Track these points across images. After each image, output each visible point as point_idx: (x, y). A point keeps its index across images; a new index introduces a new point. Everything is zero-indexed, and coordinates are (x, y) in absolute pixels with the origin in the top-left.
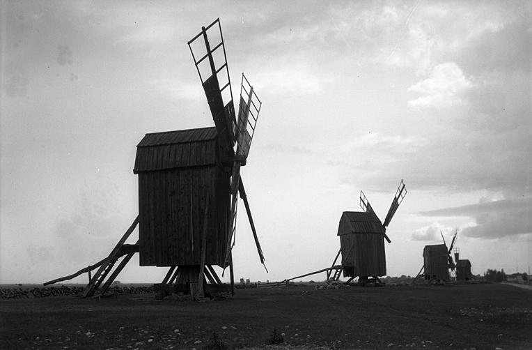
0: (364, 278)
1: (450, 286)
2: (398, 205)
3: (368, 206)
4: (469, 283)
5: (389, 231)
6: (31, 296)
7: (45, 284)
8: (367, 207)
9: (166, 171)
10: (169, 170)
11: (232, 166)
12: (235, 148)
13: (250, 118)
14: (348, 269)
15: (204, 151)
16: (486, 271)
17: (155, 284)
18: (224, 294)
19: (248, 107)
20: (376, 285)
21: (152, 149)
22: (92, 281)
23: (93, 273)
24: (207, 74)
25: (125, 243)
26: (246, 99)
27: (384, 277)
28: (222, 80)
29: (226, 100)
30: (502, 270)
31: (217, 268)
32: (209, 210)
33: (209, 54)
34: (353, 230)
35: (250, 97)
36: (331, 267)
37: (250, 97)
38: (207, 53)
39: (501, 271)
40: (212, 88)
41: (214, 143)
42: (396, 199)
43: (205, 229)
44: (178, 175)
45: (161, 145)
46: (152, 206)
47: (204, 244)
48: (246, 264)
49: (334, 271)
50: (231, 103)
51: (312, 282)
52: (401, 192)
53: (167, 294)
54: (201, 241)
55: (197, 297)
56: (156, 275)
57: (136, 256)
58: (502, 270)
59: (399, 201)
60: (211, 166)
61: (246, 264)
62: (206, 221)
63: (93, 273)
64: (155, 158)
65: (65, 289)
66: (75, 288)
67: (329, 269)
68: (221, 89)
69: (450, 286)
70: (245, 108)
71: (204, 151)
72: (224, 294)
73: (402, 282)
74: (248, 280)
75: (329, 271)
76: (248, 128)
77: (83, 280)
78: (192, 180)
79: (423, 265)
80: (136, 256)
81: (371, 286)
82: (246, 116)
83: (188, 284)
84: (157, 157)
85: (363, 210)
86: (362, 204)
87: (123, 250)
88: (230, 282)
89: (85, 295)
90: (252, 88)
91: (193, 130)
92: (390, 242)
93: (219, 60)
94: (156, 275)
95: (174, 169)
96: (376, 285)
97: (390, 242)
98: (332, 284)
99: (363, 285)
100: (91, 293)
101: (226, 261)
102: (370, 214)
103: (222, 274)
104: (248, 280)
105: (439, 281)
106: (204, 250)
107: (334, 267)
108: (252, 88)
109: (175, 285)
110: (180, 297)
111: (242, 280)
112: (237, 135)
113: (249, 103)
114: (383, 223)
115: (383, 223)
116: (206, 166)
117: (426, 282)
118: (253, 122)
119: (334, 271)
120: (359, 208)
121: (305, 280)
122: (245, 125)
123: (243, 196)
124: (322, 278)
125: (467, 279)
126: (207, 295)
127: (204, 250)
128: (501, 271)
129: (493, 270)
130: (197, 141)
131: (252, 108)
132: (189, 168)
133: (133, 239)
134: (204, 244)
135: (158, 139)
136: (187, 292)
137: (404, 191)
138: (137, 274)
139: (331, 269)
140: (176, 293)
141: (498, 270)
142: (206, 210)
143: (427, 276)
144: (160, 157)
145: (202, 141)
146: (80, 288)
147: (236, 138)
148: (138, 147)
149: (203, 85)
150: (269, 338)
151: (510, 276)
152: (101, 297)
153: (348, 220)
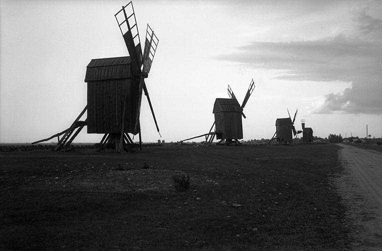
0: (229, 140)
1: (293, 146)
2: (250, 95)
3: (233, 95)
4: (311, 144)
5: (245, 111)
6: (20, 151)
7: (32, 144)
8: (232, 95)
9: (103, 81)
10: (104, 80)
11: (140, 78)
12: (142, 68)
13: (151, 49)
14: (219, 135)
15: (124, 70)
16: (329, 135)
17: (96, 144)
18: (135, 149)
19: (150, 43)
20: (237, 145)
21: (95, 68)
22: (60, 142)
23: (61, 137)
24: (125, 30)
25: (79, 120)
26: (149, 39)
27: (241, 140)
28: (134, 32)
29: (136, 43)
30: (340, 135)
31: (131, 135)
32: (126, 102)
33: (127, 20)
34: (222, 110)
35: (152, 37)
36: (208, 133)
37: (152, 37)
38: (125, 19)
39: (339, 135)
40: (128, 38)
41: (130, 66)
42: (249, 91)
43: (124, 113)
44: (110, 83)
45: (100, 66)
46: (95, 100)
47: (123, 122)
48: (149, 133)
49: (210, 136)
50: (140, 44)
51: (193, 143)
52: (252, 87)
53: (103, 149)
54: (122, 119)
55: (119, 151)
56: (96, 138)
57: (85, 127)
58: (340, 135)
59: (250, 92)
60: (127, 78)
61: (149, 133)
62: (124, 108)
63: (61, 137)
64: (97, 73)
65: (41, 147)
66: (46, 146)
67: (207, 134)
68: (133, 37)
69: (293, 146)
70: (148, 45)
71: (124, 70)
72: (135, 149)
73: (264, 143)
74: (163, 141)
75: (207, 136)
76: (150, 56)
77: (55, 140)
78: (117, 86)
79: (275, 131)
80: (85, 127)
81: (233, 145)
82: (149, 49)
83: (114, 143)
84: (98, 73)
85: (228, 97)
86: (229, 93)
87: (78, 124)
88: (139, 141)
89: (56, 150)
90: (153, 32)
91: (118, 58)
92: (245, 117)
93: (132, 22)
94: (96, 138)
95: (108, 80)
96: (237, 145)
97: (245, 117)
98: (206, 147)
99: (228, 145)
100: (59, 149)
101: (137, 130)
102: (234, 100)
103: (135, 139)
104: (163, 141)
105: (286, 142)
106: (123, 124)
107: (210, 133)
108: (153, 32)
109: (107, 144)
110: (110, 151)
111: (159, 141)
112: (143, 61)
113: (151, 41)
114: (241, 106)
115: (241, 106)
116: (125, 79)
117: (278, 143)
118: (156, 41)
119: (210, 136)
120: (227, 96)
121: (191, 141)
122: (148, 54)
123: (147, 94)
124: (203, 139)
125: (310, 141)
126: (125, 150)
127: (123, 124)
128: (339, 135)
129: (334, 134)
130: (120, 65)
131: (153, 44)
132: (116, 79)
133: (84, 118)
134: (123, 122)
135: (99, 62)
136: (114, 148)
137: (253, 86)
138: (85, 137)
139: (209, 134)
140: (108, 148)
141: (337, 135)
142: (125, 103)
143: (278, 139)
144: (100, 73)
145: (124, 65)
146: (22, 146)
147: (143, 62)
148: (88, 67)
149: (123, 36)
150: (143, 166)
151: (346, 139)
152: (65, 151)
153: (219, 104)
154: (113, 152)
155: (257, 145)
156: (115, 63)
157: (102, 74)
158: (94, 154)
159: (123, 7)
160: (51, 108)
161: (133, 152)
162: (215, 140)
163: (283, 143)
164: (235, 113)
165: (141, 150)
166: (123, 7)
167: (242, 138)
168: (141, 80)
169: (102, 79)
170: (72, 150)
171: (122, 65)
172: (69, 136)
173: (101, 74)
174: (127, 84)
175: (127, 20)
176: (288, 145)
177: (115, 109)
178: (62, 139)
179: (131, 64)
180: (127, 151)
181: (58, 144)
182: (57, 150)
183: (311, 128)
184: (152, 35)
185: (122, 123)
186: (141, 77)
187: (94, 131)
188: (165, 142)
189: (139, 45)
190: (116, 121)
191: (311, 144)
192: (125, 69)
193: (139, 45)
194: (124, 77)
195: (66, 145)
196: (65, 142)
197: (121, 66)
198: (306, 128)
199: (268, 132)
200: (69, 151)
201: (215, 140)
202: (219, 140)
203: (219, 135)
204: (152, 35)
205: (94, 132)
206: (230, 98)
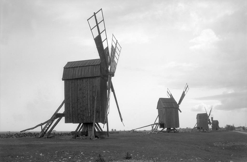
0: (169, 129)
2: (185, 95)
3: (171, 95)
5: (181, 107)
6: (14, 137)
7: (21, 132)
8: (170, 96)
12: (109, 69)
13: (116, 54)
17: (72, 132)
18: (104, 136)
19: (115, 50)
20: (175, 132)
21: (71, 69)
22: (43, 130)
23: (43, 126)
24: (96, 34)
26: (114, 46)
28: (103, 37)
29: (105, 47)
31: (101, 124)
33: (97, 25)
34: (164, 106)
35: (116, 45)
37: (116, 45)
39: (232, 125)
42: (184, 92)
45: (75, 67)
46: (71, 96)
47: (95, 113)
48: (114, 123)
49: (155, 125)
53: (78, 136)
54: (93, 111)
56: (73, 127)
57: (63, 119)
59: (185, 93)
60: (98, 77)
61: (114, 123)
63: (43, 126)
64: (72, 73)
65: (30, 134)
67: (153, 125)
68: (102, 41)
70: (114, 50)
72: (104, 136)
73: (187, 131)
74: (115, 130)
75: (153, 125)
76: (115, 59)
78: (89, 86)
80: (63, 119)
81: (172, 132)
82: (114, 53)
86: (168, 94)
87: (57, 116)
88: (106, 130)
90: (117, 41)
92: (181, 112)
93: (101, 27)
94: (73, 127)
96: (175, 132)
97: (181, 112)
98: (154, 133)
99: (169, 132)
100: (42, 136)
101: (105, 120)
102: (172, 100)
103: (103, 127)
104: (115, 130)
105: (204, 130)
106: (95, 116)
107: (155, 124)
108: (117, 41)
109: (81, 132)
112: (110, 62)
114: (178, 103)
115: (178, 103)
116: (95, 77)
117: (198, 130)
120: (167, 97)
122: (114, 58)
123: (113, 91)
125: (217, 129)
126: (96, 137)
127: (95, 116)
129: (229, 125)
130: (91, 65)
131: (117, 50)
133: (62, 111)
134: (95, 113)
136: (87, 135)
139: (154, 125)
141: (231, 125)
142: (96, 97)
143: (198, 128)
144: (74, 73)
150: (125, 156)
153: (162, 102)
154: (86, 139)
155: (183, 132)
156: (87, 65)
157: (77, 73)
158: (71, 140)
159: (94, 13)
160: (32, 102)
161: (103, 138)
162: (160, 129)
163: (202, 130)
164: (174, 109)
165: (108, 136)
166: (94, 13)
167: (179, 127)
168: (108, 78)
169: (76, 78)
170: (52, 137)
171: (93, 65)
172: (50, 126)
173: (75, 74)
174: (97, 82)
175: (97, 25)
176: (205, 132)
177: (88, 102)
178: (44, 128)
179: (100, 64)
180: (98, 138)
181: (41, 132)
182: (40, 137)
183: (217, 121)
184: (116, 43)
185: (93, 114)
186: (109, 76)
187: (70, 121)
188: (117, 130)
189: (107, 48)
190: (89, 113)
191: (217, 131)
192: (96, 69)
193: (107, 48)
194: (95, 76)
195: (48, 133)
196: (46, 130)
197: (93, 67)
198: (214, 121)
199: (111, 130)
200: (51, 137)
201: (160, 129)
202: (162, 129)
203: (162, 125)
204: (116, 43)
205: (70, 122)
206: (169, 98)
